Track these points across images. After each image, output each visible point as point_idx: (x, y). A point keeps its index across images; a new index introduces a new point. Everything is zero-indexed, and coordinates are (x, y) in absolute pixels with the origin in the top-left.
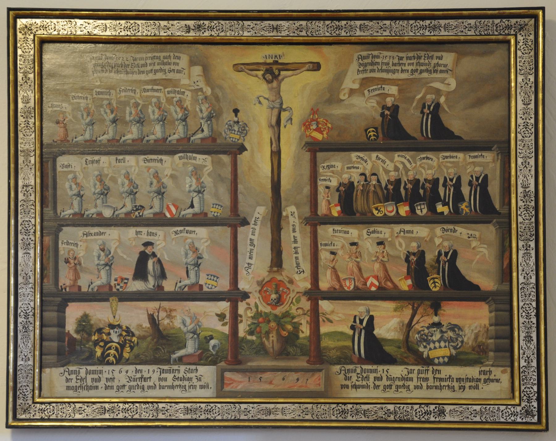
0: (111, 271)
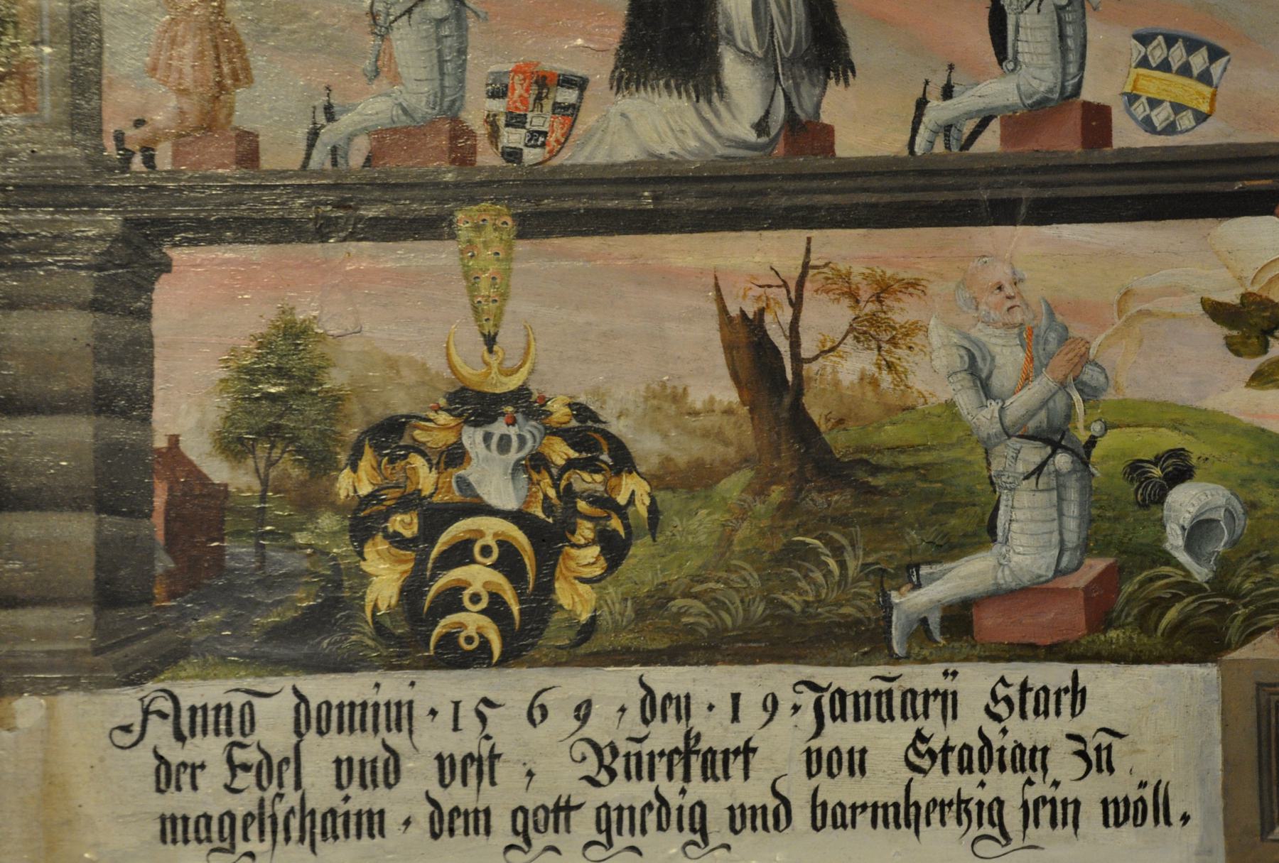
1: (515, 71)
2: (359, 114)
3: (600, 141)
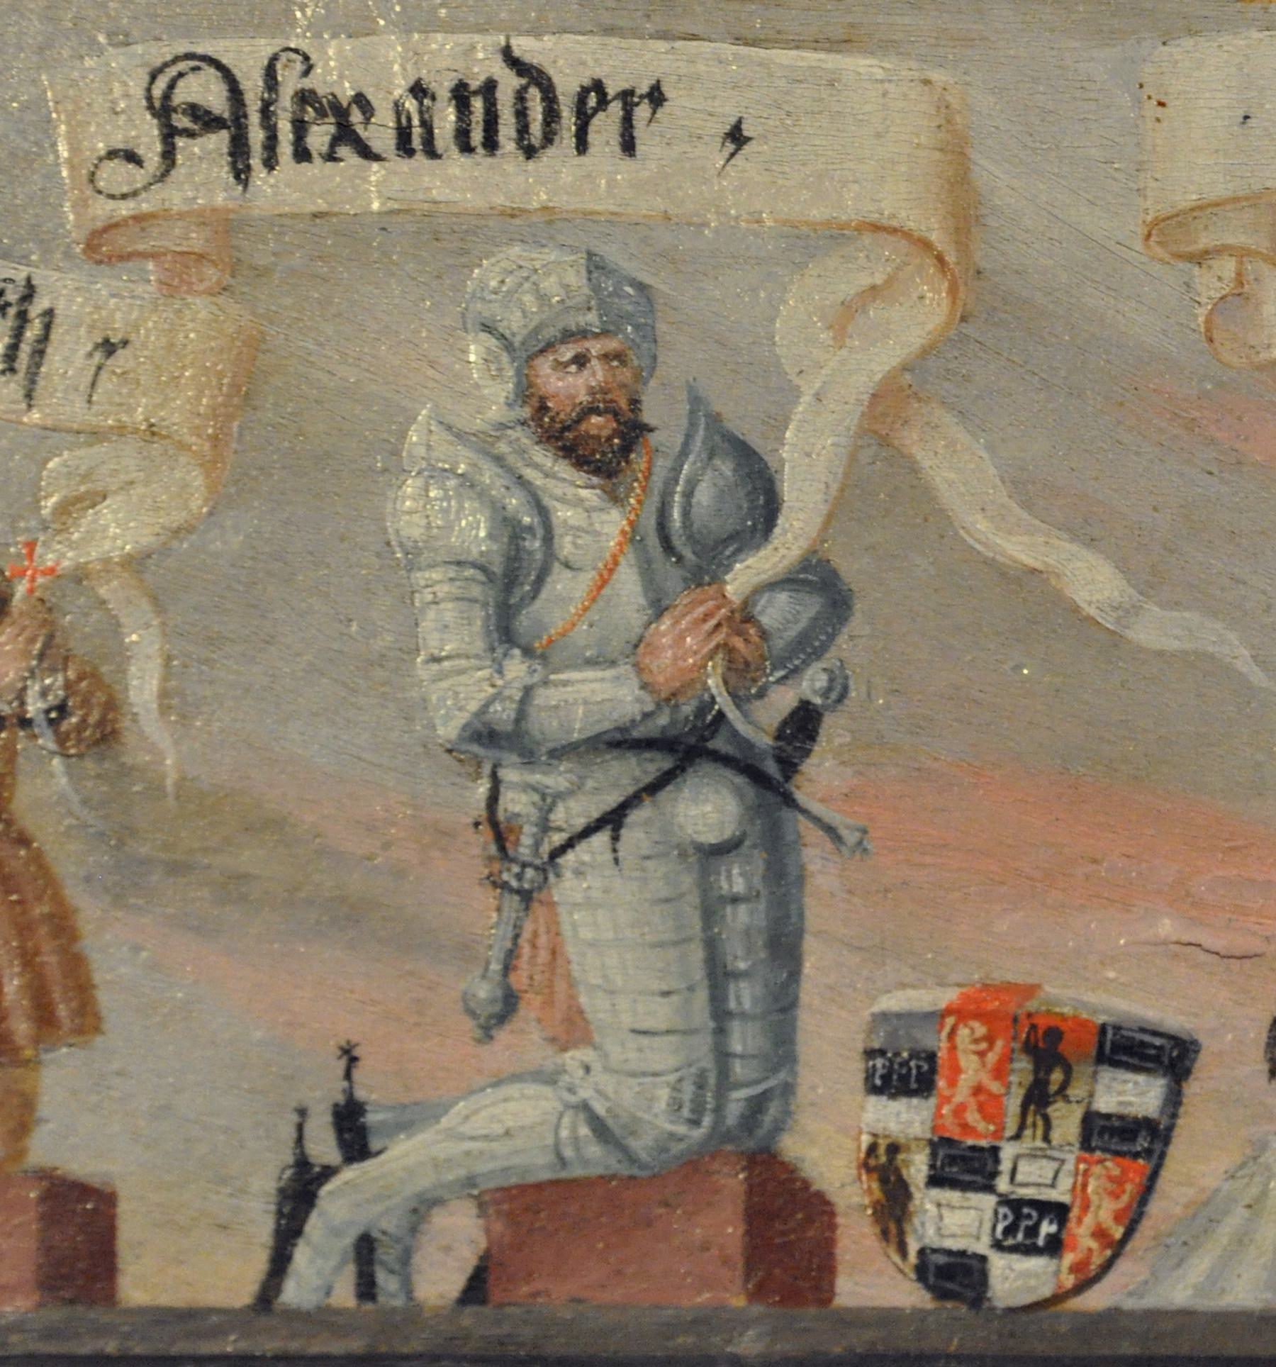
0: (783, 880)
1: (960, 1013)
2: (453, 1135)
3: (1242, 1240)
